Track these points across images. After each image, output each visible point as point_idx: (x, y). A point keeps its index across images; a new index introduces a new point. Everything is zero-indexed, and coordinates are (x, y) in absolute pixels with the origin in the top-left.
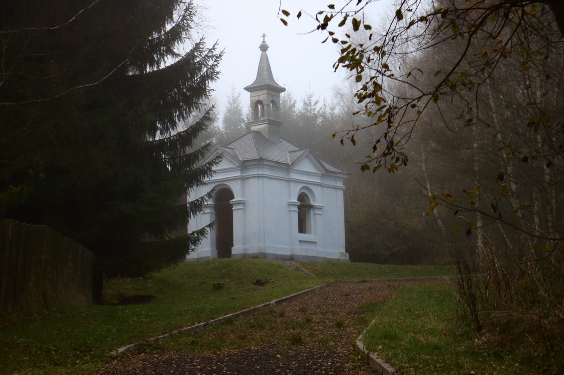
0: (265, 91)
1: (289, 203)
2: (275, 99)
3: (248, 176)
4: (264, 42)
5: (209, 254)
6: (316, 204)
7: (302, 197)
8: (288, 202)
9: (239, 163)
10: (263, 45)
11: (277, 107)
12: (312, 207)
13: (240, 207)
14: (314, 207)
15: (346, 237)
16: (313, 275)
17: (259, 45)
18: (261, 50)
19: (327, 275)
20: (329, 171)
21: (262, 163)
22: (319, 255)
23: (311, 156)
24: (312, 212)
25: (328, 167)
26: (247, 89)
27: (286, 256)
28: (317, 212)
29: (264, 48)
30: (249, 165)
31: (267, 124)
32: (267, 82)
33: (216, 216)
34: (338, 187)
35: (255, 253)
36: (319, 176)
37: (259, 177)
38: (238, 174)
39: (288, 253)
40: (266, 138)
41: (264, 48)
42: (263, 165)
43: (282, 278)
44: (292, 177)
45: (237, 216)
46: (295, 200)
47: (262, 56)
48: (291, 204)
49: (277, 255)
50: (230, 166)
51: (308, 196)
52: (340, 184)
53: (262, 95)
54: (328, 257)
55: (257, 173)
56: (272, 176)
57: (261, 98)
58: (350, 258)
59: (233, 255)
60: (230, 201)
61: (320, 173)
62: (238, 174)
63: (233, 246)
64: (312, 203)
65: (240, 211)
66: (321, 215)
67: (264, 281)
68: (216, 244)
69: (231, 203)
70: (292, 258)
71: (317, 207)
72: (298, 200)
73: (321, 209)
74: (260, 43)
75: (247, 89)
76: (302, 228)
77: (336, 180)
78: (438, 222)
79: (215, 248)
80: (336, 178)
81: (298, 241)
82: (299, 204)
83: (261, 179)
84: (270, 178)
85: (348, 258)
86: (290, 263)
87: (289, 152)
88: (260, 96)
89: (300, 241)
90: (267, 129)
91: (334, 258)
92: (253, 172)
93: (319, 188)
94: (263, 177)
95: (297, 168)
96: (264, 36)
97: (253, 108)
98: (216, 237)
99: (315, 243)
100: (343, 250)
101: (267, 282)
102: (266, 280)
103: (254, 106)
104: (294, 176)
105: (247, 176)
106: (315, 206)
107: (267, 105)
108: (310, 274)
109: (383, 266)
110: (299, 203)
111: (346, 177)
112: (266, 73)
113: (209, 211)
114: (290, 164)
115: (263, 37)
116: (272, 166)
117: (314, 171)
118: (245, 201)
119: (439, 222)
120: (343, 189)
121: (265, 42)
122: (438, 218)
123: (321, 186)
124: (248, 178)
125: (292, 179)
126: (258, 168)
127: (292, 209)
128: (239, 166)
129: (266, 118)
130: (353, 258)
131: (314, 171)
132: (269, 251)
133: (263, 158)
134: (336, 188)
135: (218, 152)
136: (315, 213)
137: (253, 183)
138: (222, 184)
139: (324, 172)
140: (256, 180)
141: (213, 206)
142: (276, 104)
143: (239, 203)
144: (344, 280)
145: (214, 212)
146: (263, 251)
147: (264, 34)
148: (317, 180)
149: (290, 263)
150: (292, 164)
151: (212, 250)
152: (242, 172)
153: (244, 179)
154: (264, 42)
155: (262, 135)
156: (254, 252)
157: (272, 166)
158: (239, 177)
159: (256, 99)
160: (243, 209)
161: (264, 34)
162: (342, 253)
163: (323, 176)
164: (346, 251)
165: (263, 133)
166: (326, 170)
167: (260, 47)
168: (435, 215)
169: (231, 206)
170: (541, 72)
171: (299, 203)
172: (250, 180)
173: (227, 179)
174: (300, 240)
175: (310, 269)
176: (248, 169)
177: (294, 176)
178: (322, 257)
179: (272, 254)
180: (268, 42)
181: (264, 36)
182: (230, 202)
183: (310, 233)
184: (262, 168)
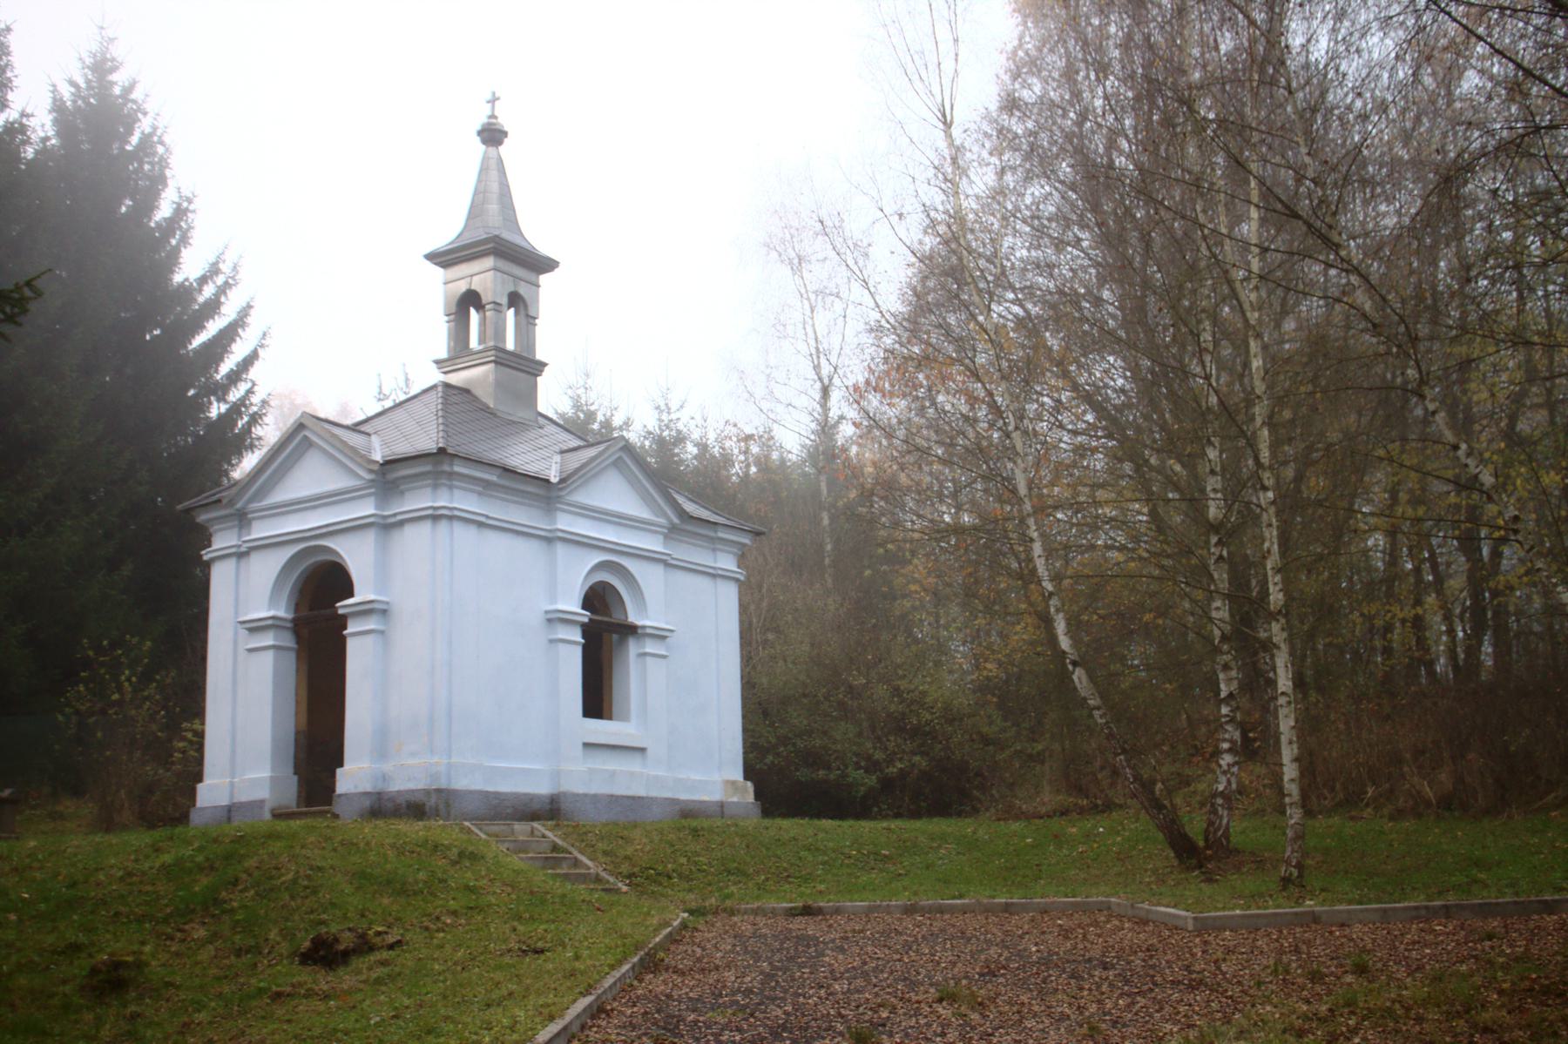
0: (489, 262)
1: (549, 616)
2: (523, 290)
3: (400, 517)
4: (493, 116)
5: (263, 793)
6: (648, 623)
7: (598, 598)
8: (547, 612)
9: (371, 471)
10: (489, 124)
11: (528, 316)
12: (632, 630)
13: (371, 624)
14: (640, 631)
15: (745, 730)
16: (612, 879)
17: (479, 127)
18: (484, 142)
19: (670, 877)
20: (692, 517)
21: (446, 468)
22: (654, 793)
23: (629, 462)
24: (633, 647)
25: (690, 507)
26: (433, 257)
27: (531, 798)
28: (650, 647)
29: (492, 135)
30: (404, 477)
31: (492, 366)
32: (494, 222)
33: (298, 658)
34: (720, 572)
35: (413, 791)
36: (656, 532)
37: (435, 517)
38: (365, 509)
39: (541, 787)
40: (488, 407)
41: (492, 135)
42: (451, 475)
43: (454, 913)
44: (560, 526)
45: (359, 656)
46: (572, 604)
47: (485, 159)
48: (556, 619)
49: (497, 795)
50: (334, 481)
51: (613, 587)
52: (727, 563)
53: (482, 276)
54: (684, 796)
55: (430, 504)
56: (487, 517)
57: (476, 284)
58: (758, 795)
59: (340, 795)
60: (338, 604)
61: (662, 521)
62: (365, 509)
63: (341, 765)
64: (633, 618)
65: (369, 639)
66: (664, 657)
67: (347, 940)
68: (296, 757)
69: (340, 612)
70: (551, 810)
71: (649, 631)
72: (584, 607)
73: (664, 638)
74: (481, 120)
75: (433, 257)
76: (597, 701)
77: (714, 550)
78: (1075, 677)
79: (288, 770)
80: (714, 544)
81: (581, 747)
82: (586, 620)
83: (443, 526)
84: (481, 525)
85: (750, 797)
86: (532, 833)
87: (562, 452)
88: (475, 278)
89: (587, 746)
90: (491, 378)
91: (706, 798)
92: (418, 500)
93: (659, 570)
94: (451, 518)
95: (583, 497)
96: (493, 100)
97: (452, 317)
98: (297, 733)
99: (642, 750)
100: (737, 774)
101: (364, 946)
102: (363, 936)
103: (453, 309)
104: (566, 523)
105: (395, 515)
106: (644, 627)
107: (494, 303)
108: (604, 874)
109: (866, 826)
110: (585, 616)
111: (746, 540)
112: (493, 207)
113: (271, 642)
114: (554, 480)
115: (490, 105)
116: (487, 484)
117: (641, 512)
118: (387, 603)
119: (1079, 676)
120: (737, 580)
121: (496, 117)
122: (1075, 664)
123: (666, 564)
124: (401, 523)
125: (560, 534)
126: (435, 487)
127: (561, 636)
128: (372, 481)
129: (491, 344)
130: (767, 812)
131: (645, 514)
132: (462, 783)
133: (450, 450)
134: (714, 575)
135: (305, 437)
136: (641, 651)
137: (416, 538)
138: (315, 547)
139: (676, 520)
140: (425, 528)
141: (289, 625)
142: (526, 306)
143: (367, 610)
144: (728, 903)
145: (295, 646)
146: (443, 784)
147: (494, 94)
148: (653, 544)
149: (532, 833)
150: (562, 481)
151: (274, 780)
152: (377, 508)
153: (387, 527)
154: (493, 116)
155: (476, 399)
156: (411, 786)
157: (487, 484)
158: (371, 520)
159: (462, 287)
160: (382, 632)
161: (494, 94)
162: (733, 783)
163: (672, 533)
164: (746, 778)
165: (478, 392)
166: (683, 514)
167: (480, 133)
168: (1064, 652)
169: (342, 621)
170: (1368, 195)
171: (585, 616)
172: (410, 532)
173: (331, 529)
174: (586, 740)
175: (605, 853)
176: (402, 493)
177: (566, 523)
178: (666, 799)
179: (480, 792)
180: (505, 121)
181: (493, 100)
182: (337, 609)
183: (625, 718)
184: (451, 488)
